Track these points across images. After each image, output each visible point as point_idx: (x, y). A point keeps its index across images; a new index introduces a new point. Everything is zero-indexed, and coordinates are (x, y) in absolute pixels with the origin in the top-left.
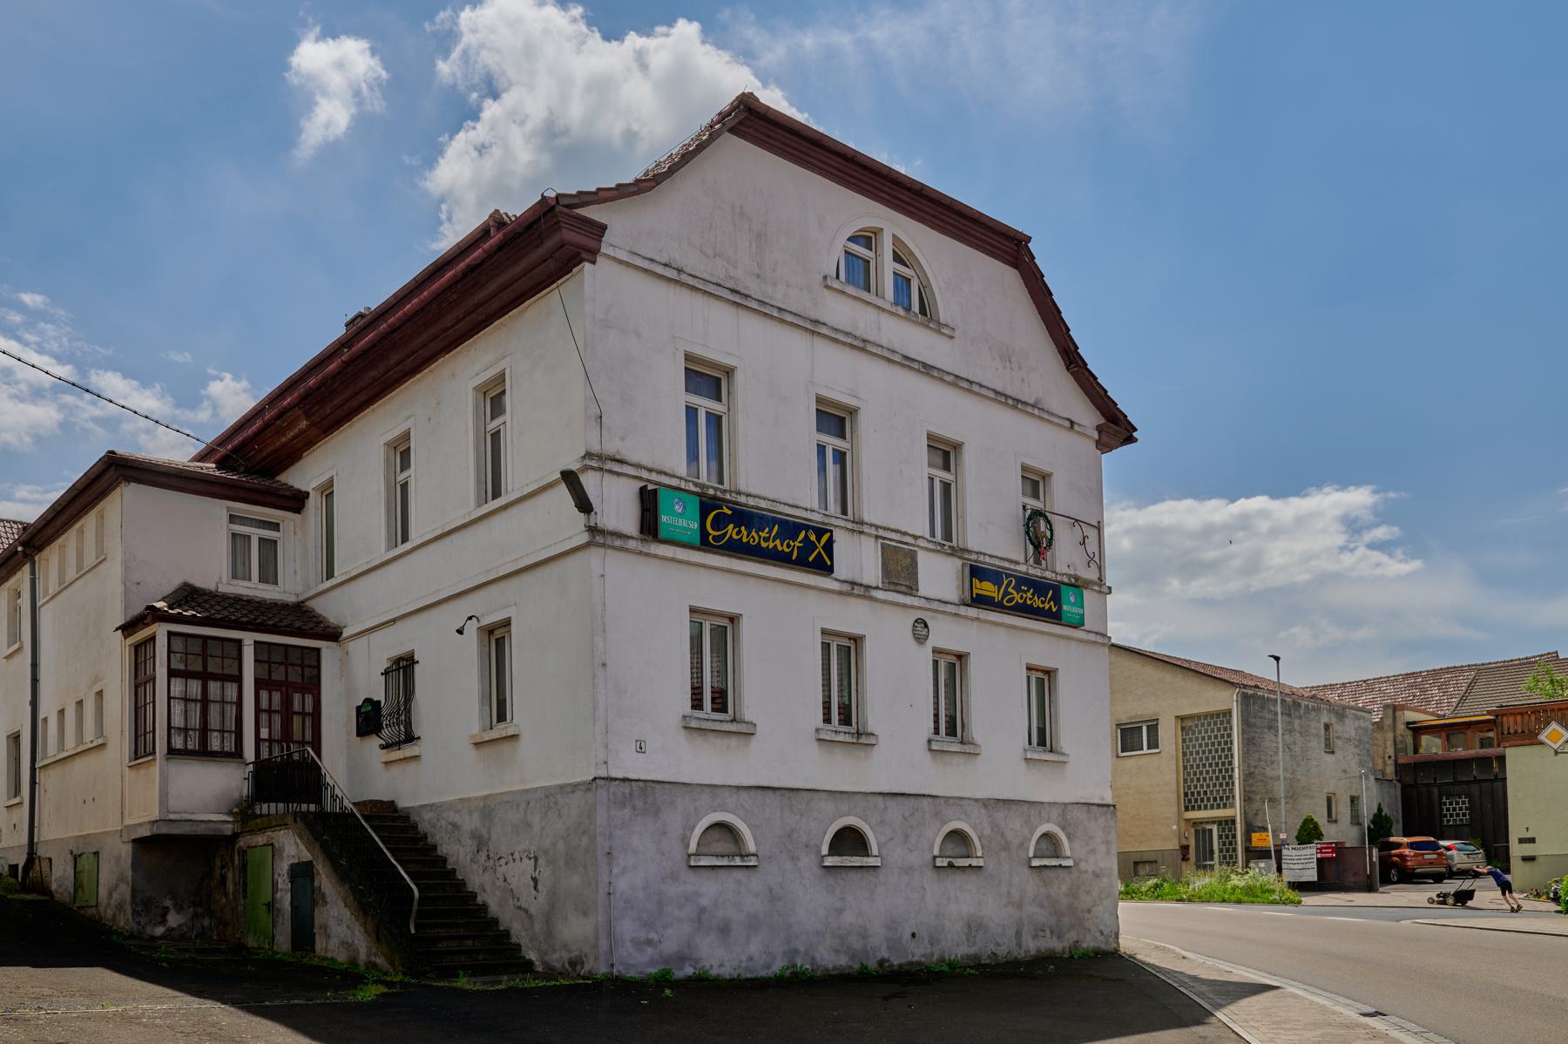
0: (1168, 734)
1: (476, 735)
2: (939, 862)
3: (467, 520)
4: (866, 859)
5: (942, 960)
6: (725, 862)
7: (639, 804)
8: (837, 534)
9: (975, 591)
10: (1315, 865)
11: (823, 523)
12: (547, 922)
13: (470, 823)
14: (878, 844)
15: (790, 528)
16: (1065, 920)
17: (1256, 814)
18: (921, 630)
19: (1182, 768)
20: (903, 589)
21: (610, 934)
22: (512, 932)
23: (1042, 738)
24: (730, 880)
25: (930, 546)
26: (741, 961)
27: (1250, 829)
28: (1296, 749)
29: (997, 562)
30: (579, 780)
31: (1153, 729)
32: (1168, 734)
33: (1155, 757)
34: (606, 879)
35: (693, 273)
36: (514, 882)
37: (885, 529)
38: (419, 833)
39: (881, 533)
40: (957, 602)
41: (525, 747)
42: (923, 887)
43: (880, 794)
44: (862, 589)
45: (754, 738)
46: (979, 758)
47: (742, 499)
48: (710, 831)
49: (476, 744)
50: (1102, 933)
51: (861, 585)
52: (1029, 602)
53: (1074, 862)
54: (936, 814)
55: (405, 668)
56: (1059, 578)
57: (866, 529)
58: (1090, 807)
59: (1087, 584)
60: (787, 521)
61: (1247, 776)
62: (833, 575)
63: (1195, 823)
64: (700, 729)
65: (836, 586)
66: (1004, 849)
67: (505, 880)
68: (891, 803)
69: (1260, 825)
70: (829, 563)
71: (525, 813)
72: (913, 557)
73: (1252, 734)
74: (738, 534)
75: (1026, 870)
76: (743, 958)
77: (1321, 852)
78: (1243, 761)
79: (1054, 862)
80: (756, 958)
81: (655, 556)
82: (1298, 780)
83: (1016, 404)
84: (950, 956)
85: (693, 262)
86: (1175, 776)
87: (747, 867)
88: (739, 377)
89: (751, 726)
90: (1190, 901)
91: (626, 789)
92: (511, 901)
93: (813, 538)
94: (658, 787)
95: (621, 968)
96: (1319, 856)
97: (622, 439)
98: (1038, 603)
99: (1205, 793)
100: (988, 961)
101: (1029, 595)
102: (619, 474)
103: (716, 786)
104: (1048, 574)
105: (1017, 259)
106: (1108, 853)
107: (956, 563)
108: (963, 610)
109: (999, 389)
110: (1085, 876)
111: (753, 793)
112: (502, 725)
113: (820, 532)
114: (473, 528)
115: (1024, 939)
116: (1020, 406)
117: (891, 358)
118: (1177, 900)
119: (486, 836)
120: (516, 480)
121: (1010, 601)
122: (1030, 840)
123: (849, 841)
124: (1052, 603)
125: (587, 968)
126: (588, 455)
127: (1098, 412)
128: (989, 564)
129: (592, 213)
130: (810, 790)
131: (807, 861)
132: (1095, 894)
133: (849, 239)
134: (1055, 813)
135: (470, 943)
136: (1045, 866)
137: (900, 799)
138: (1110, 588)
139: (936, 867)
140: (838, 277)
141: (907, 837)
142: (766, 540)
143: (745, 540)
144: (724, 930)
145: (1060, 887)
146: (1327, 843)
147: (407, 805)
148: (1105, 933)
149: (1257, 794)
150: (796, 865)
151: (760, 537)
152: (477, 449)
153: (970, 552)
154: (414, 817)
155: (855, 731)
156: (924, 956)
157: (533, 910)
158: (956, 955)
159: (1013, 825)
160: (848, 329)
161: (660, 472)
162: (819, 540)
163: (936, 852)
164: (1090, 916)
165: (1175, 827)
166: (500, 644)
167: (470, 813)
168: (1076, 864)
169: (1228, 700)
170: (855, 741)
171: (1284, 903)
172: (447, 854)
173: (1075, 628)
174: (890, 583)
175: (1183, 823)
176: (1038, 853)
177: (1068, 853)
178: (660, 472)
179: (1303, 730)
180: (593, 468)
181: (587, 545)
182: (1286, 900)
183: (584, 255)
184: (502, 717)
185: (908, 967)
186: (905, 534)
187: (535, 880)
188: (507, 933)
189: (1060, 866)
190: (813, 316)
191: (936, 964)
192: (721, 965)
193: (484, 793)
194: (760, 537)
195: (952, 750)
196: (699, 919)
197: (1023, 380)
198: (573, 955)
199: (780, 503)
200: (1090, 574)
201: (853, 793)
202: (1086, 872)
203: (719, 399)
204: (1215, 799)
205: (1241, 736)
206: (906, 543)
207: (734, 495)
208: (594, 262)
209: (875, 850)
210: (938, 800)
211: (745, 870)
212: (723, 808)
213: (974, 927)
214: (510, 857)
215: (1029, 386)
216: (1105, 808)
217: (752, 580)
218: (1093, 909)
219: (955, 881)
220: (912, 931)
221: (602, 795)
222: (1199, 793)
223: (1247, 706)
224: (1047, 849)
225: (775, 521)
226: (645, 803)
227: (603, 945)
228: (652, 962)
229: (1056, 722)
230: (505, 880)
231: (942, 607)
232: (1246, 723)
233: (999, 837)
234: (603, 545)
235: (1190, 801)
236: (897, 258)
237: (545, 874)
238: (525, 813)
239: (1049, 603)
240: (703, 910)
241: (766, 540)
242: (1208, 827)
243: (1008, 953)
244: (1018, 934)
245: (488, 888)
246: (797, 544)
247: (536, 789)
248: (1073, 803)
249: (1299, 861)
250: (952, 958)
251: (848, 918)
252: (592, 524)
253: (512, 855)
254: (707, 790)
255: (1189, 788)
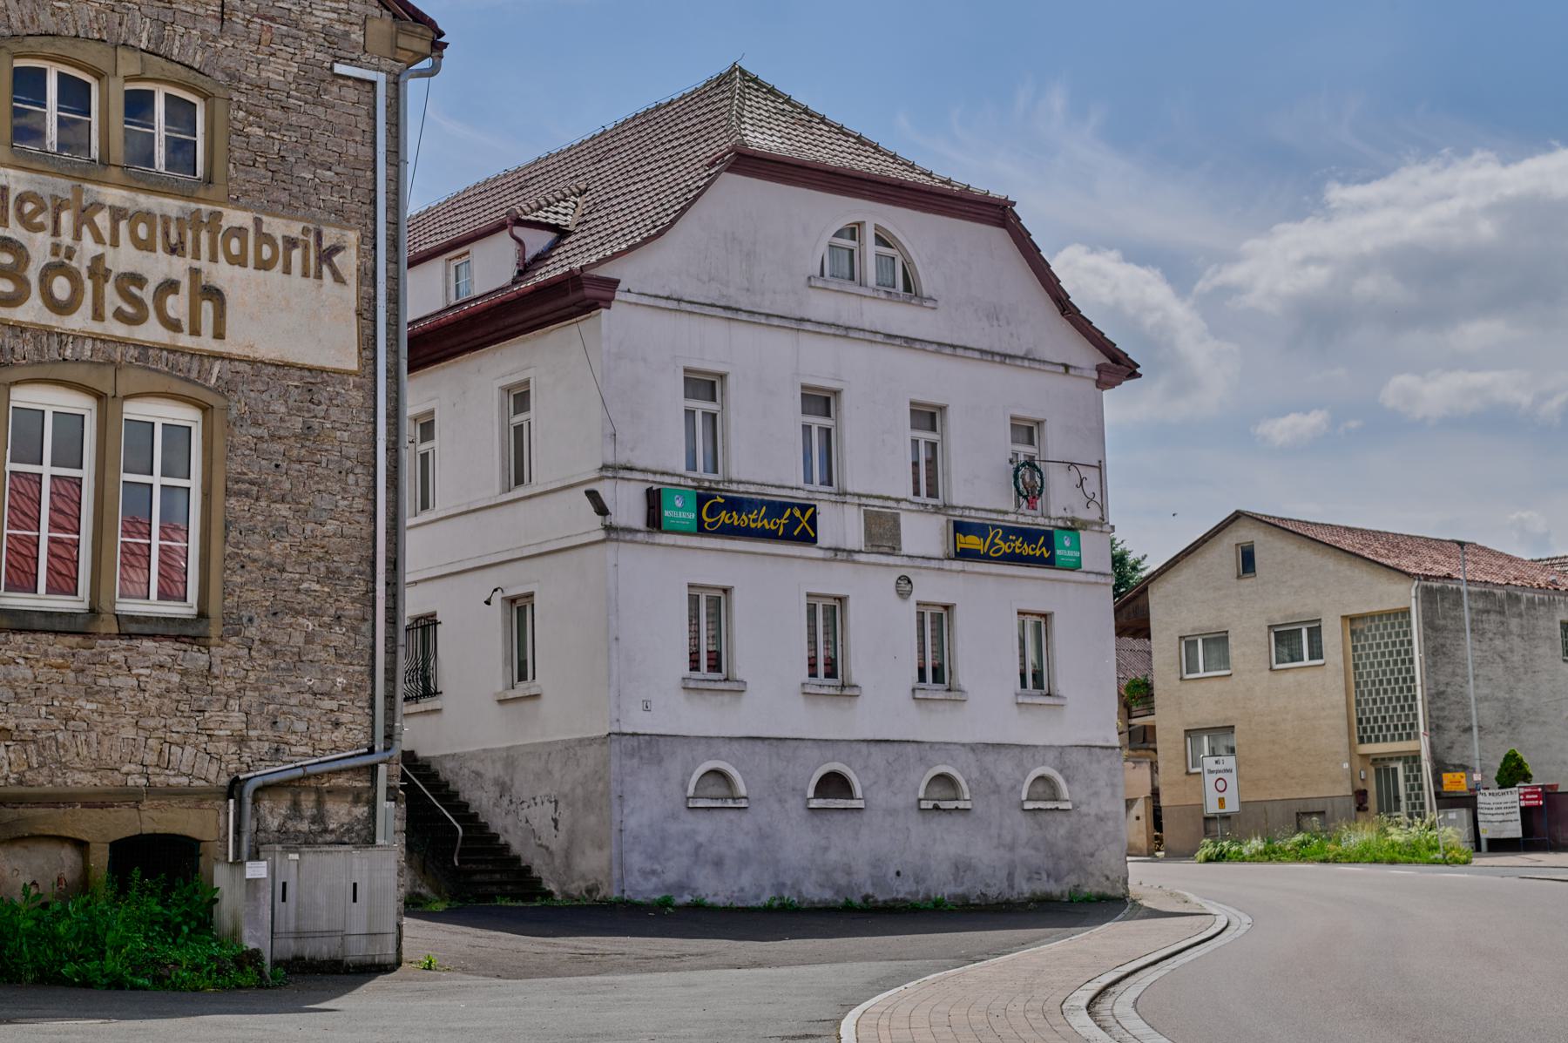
0: (1333, 637)
1: (500, 693)
2: (924, 805)
3: (493, 503)
4: (849, 801)
5: (928, 898)
6: (718, 804)
7: (646, 754)
8: (821, 507)
9: (959, 546)
10: (1518, 816)
11: (808, 499)
12: (567, 857)
13: (492, 771)
14: (862, 787)
15: (776, 508)
16: (1064, 864)
17: (1450, 748)
18: (904, 586)
19: (1353, 685)
20: (886, 550)
21: (621, 865)
22: (534, 867)
23: (1036, 679)
24: (722, 819)
25: (913, 507)
26: (733, 892)
27: (1440, 768)
28: (1515, 659)
29: (984, 515)
30: (595, 734)
31: (1315, 633)
32: (1333, 637)
33: (1318, 671)
34: (618, 819)
35: (692, 299)
36: (535, 823)
37: (868, 496)
38: (439, 781)
39: (864, 501)
40: (941, 556)
41: (546, 706)
42: (908, 828)
43: (863, 741)
44: (845, 554)
45: (744, 694)
46: (966, 704)
47: (734, 487)
48: (707, 777)
49: (500, 701)
50: (1108, 878)
51: (844, 550)
52: (1017, 551)
53: (1073, 805)
54: (921, 759)
55: (423, 627)
56: (1053, 523)
57: (848, 498)
58: (1093, 749)
59: (1085, 525)
60: (774, 502)
61: (1433, 698)
62: (818, 544)
63: (1375, 760)
64: (698, 689)
65: (820, 554)
66: (994, 792)
67: (527, 821)
68: (874, 749)
69: (1457, 762)
70: (813, 535)
71: (547, 763)
72: (895, 519)
73: (1441, 641)
74: (729, 519)
75: (1019, 814)
76: (736, 889)
77: (1525, 799)
78: (1427, 677)
79: (1050, 805)
80: (747, 889)
81: (659, 544)
82: (1519, 701)
83: (1005, 358)
84: (936, 894)
85: (691, 291)
86: (1344, 697)
87: (739, 808)
88: (731, 380)
89: (741, 684)
90: (1335, 861)
91: (634, 742)
92: (532, 840)
93: (798, 514)
94: (661, 739)
95: (630, 893)
96: (1523, 804)
97: (632, 450)
98: (1027, 550)
99: (1384, 718)
100: (977, 901)
101: (1018, 543)
102: (629, 480)
103: (711, 738)
104: (1040, 520)
105: (1003, 220)
106: (1114, 795)
107: (941, 520)
108: (947, 564)
109: (985, 347)
110: (1086, 819)
111: (744, 742)
112: (523, 685)
113: (804, 508)
114: (499, 509)
115: (1016, 881)
116: (1008, 361)
117: (874, 339)
118: (1321, 861)
119: (509, 783)
120: (542, 472)
121: (996, 551)
122: (1023, 783)
123: (834, 784)
124: (1044, 549)
125: (602, 893)
126: (605, 467)
127: (1098, 352)
128: (975, 518)
129: (605, 272)
130: (796, 739)
131: (794, 804)
132: (1099, 837)
133: (835, 236)
134: (1051, 755)
135: (498, 876)
136: (1040, 809)
137: (883, 745)
138: (1113, 527)
139: (921, 809)
140: (822, 274)
141: (890, 781)
142: (754, 521)
143: (736, 523)
144: (718, 863)
145: (1059, 831)
146: (1532, 787)
147: (426, 754)
148: (1111, 878)
149: (1453, 720)
150: (783, 807)
151: (749, 519)
152: (502, 440)
153: (954, 508)
154: (435, 766)
155: (840, 683)
156: (910, 893)
157: (553, 847)
158: (943, 894)
159: (1004, 768)
160: (831, 320)
161: (663, 473)
162: (803, 515)
163: (921, 794)
164: (1092, 860)
165: (1346, 766)
166: (521, 611)
167: (493, 762)
168: (1075, 807)
169: (1405, 595)
170: (838, 693)
171: (1447, 863)
172: (469, 799)
173: (1073, 570)
174: (872, 546)
175: (1357, 760)
176: (1034, 796)
177: (1067, 796)
178: (663, 473)
179: (1525, 633)
180: (608, 478)
181: (603, 541)
182: (1450, 859)
183: (601, 304)
184: (522, 676)
185: (892, 904)
186: (888, 498)
187: (555, 821)
188: (528, 869)
189: (1057, 809)
190: (798, 315)
191: (922, 902)
192: (715, 895)
193: (509, 744)
194: (749, 519)
195: (937, 697)
196: (696, 854)
197: (1012, 335)
198: (590, 883)
199: (768, 486)
200: (1093, 514)
201: (837, 741)
202: (1088, 815)
203: (714, 399)
204: (1396, 728)
205: (1422, 644)
206: (888, 508)
207: (726, 484)
208: (609, 308)
209: (858, 792)
210: (922, 746)
211: (737, 811)
212: (717, 757)
213: (961, 867)
214: (532, 801)
215: (1019, 339)
216: (1110, 751)
217: (742, 556)
218: (1097, 854)
219: (940, 824)
220: (896, 870)
221: (616, 747)
222: (1376, 720)
223: (1431, 603)
224: (1045, 792)
225: (763, 503)
226: (651, 754)
227: (616, 873)
228: (656, 890)
229: (1053, 665)
230: (527, 821)
231: (926, 563)
232: (1430, 625)
233: (988, 781)
234: (617, 540)
235: (1364, 730)
236: (880, 241)
237: (565, 815)
238: (547, 763)
239: (1040, 549)
240: (700, 846)
241: (754, 521)
242: (1393, 765)
243: (999, 894)
244: (1010, 876)
245: (511, 829)
246: (783, 521)
247: (556, 742)
248: (1071, 746)
249: (1499, 811)
250: (939, 896)
251: (833, 856)
252: (608, 523)
253: (534, 799)
254: (703, 741)
255: (1364, 712)
